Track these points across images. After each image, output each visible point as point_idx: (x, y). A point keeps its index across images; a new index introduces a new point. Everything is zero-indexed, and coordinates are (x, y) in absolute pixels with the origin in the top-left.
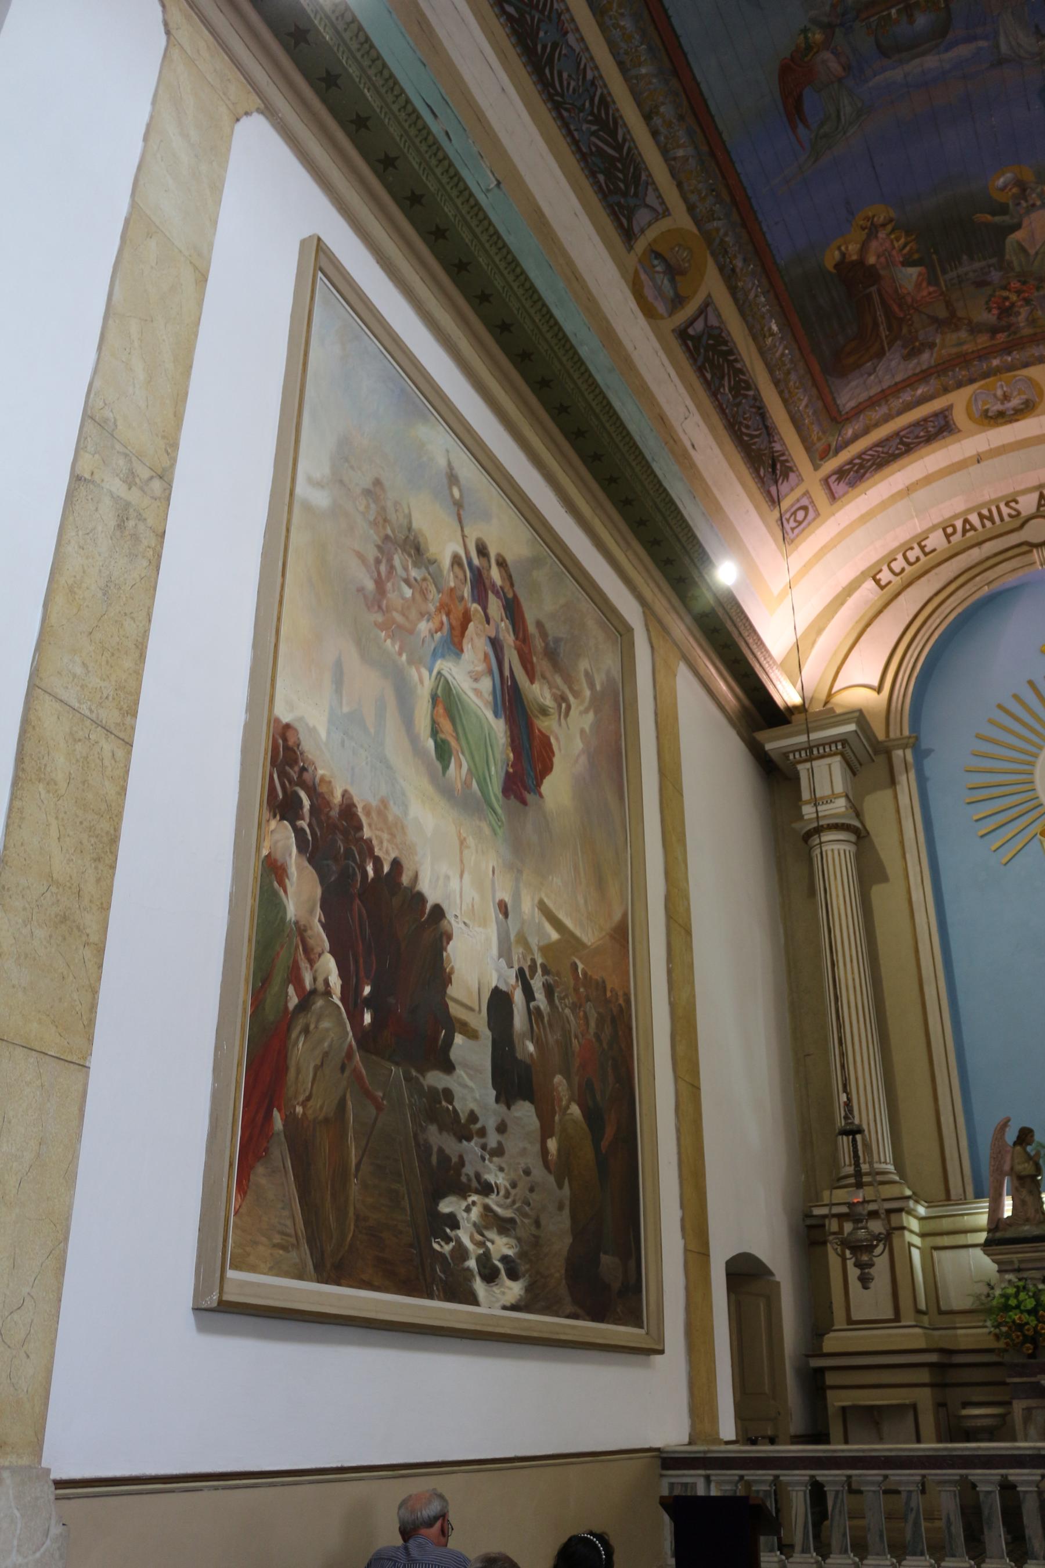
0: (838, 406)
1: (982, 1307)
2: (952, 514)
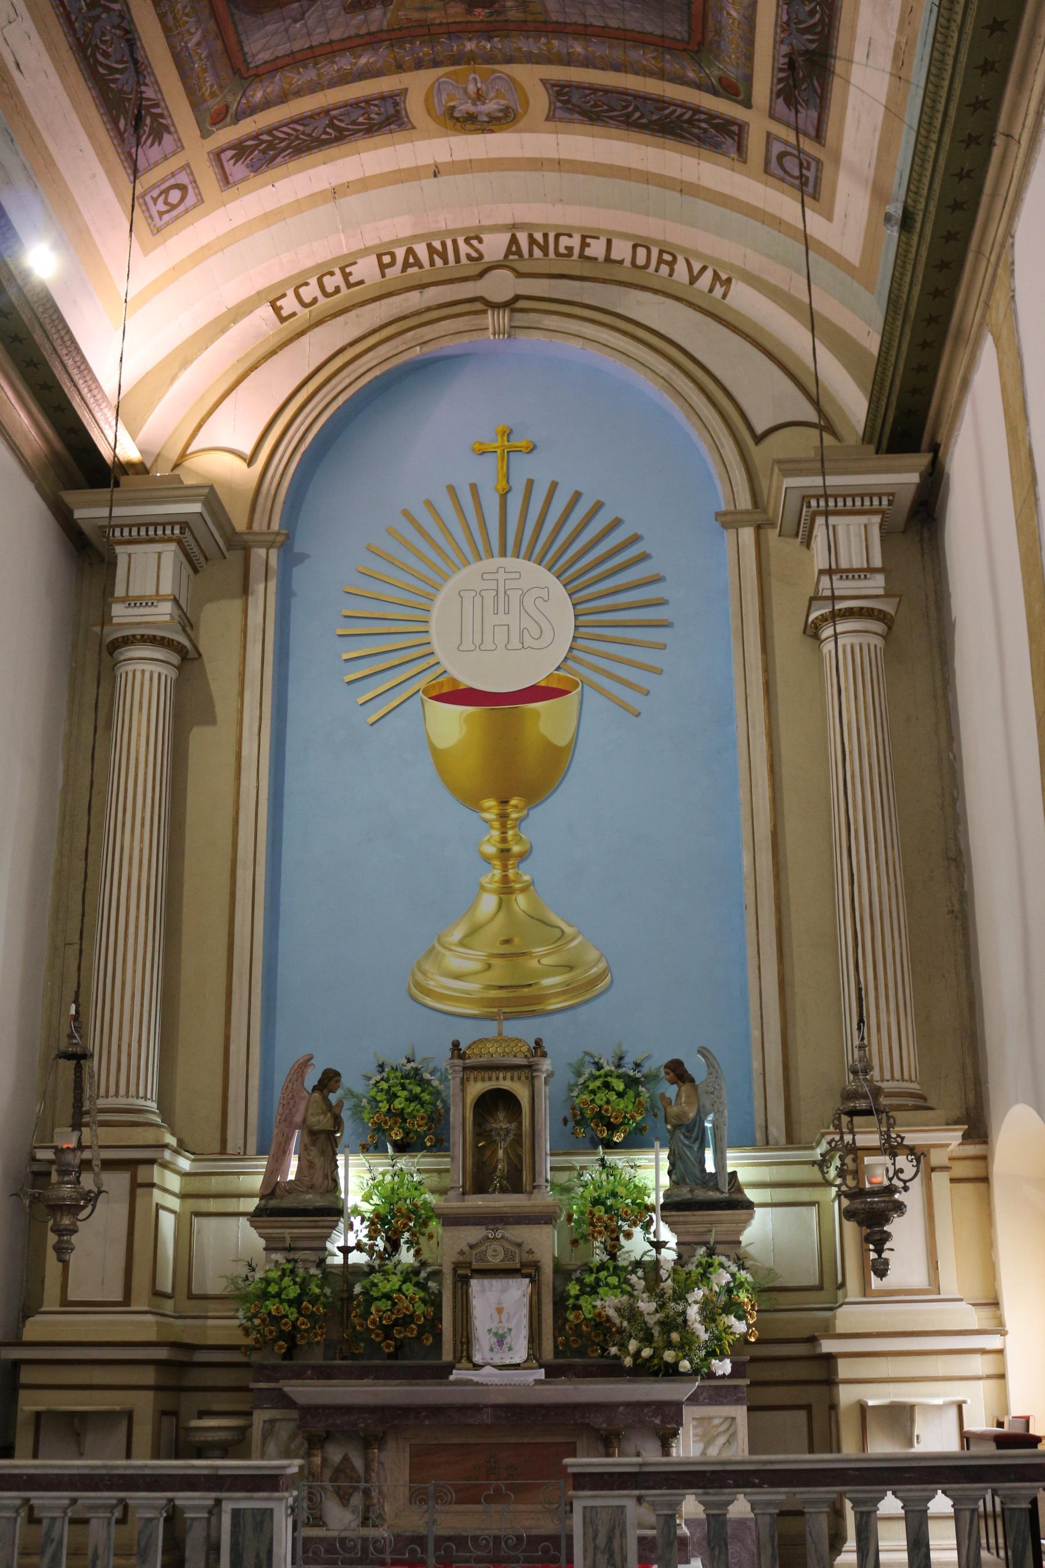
0: (244, 54)
1: (236, 1293)
2: (394, 238)
